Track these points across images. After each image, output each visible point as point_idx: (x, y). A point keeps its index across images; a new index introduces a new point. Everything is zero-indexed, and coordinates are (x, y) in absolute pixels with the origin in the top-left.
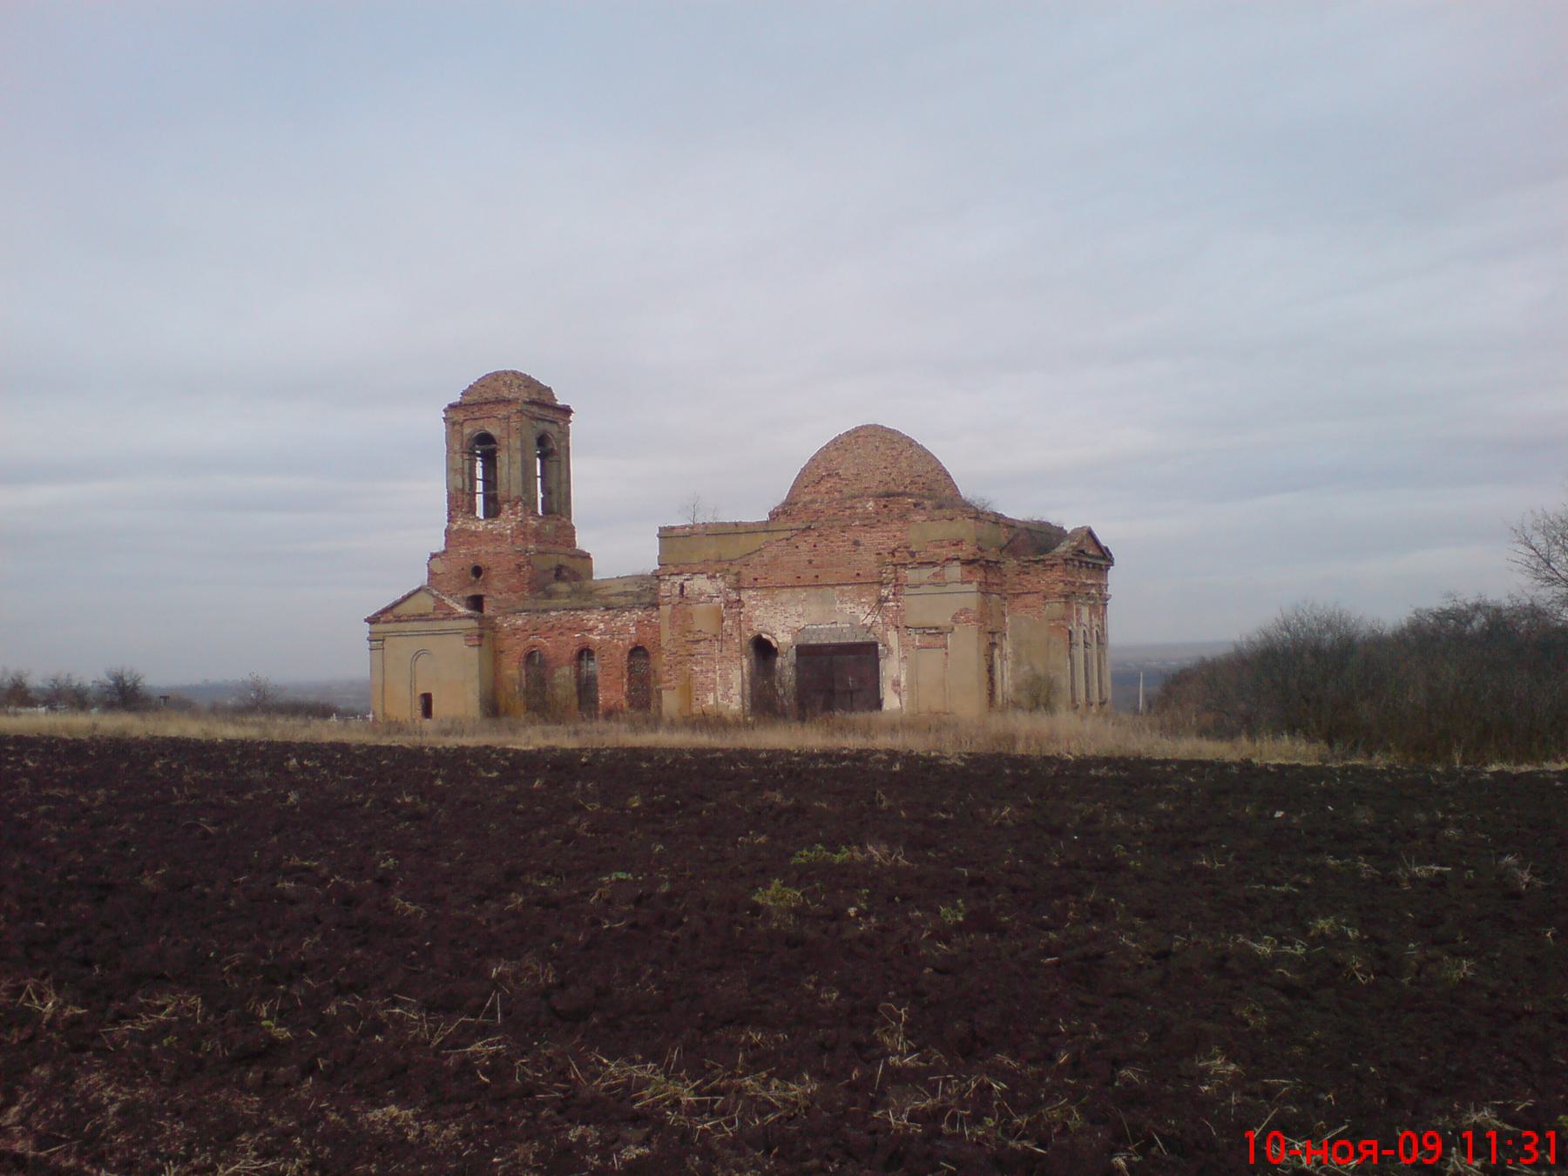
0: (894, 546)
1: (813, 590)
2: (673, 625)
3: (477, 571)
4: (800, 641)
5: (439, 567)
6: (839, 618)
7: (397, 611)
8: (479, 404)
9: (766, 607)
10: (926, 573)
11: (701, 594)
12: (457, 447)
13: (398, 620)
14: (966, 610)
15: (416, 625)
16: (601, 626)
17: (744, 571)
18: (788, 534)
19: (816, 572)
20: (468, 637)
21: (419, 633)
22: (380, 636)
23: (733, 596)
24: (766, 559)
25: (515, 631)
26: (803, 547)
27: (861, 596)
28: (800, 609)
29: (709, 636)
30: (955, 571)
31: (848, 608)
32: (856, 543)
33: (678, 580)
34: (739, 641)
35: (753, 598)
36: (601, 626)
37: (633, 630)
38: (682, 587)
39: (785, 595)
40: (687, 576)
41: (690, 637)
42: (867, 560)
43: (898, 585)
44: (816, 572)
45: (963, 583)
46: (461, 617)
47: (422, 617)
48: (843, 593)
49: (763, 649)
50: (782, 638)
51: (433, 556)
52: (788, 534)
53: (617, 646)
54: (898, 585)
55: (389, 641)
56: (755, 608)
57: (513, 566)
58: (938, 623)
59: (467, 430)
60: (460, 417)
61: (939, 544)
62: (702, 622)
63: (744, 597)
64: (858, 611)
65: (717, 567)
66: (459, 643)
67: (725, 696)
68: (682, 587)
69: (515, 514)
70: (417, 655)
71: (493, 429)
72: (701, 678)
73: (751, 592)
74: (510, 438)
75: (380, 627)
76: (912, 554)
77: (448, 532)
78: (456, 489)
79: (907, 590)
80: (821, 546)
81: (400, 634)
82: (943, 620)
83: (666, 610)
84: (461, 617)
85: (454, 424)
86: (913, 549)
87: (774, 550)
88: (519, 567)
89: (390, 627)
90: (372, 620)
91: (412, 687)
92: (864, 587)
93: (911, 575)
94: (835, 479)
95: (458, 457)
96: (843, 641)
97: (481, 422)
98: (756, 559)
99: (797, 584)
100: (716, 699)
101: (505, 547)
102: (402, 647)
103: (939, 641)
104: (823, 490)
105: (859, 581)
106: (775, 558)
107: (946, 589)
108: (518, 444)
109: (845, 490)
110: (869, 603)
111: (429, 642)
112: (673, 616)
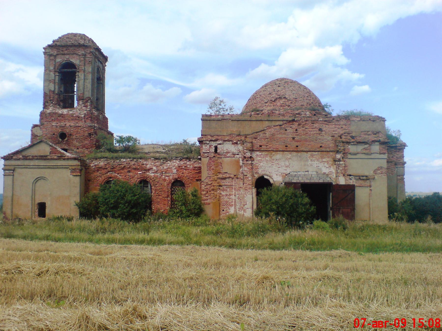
0: (341, 132)
1: (294, 154)
2: (209, 168)
3: (63, 136)
4: (287, 180)
5: (39, 132)
6: (310, 169)
7: (24, 153)
8: (66, 46)
9: (267, 161)
10: (360, 148)
11: (228, 153)
12: (52, 68)
13: (26, 158)
14: (381, 168)
15: (37, 162)
16: (154, 168)
17: (254, 141)
18: (281, 123)
19: (297, 144)
20: (73, 171)
21: (39, 167)
22: (12, 168)
23: (248, 154)
24: (267, 135)
25: (99, 169)
26: (290, 130)
27: (322, 158)
28: (287, 164)
29: (232, 176)
30: (376, 148)
31: (316, 163)
32: (320, 130)
33: (214, 144)
34: (250, 180)
35: (260, 156)
36: (154, 168)
37: (175, 171)
38: (216, 148)
39: (278, 156)
40: (220, 142)
41: (220, 176)
42: (327, 140)
43: (345, 154)
44: (297, 144)
45: (380, 154)
46: (68, 159)
47: (43, 158)
48: (312, 156)
49: (262, 183)
50: (276, 178)
51: (35, 126)
52: (281, 123)
53: (165, 180)
54: (345, 154)
55: (18, 170)
56: (260, 161)
57: (86, 134)
58: (367, 174)
59: (58, 60)
60: (55, 52)
61: (366, 133)
62: (227, 167)
63: (254, 155)
64: (321, 165)
65: (238, 138)
66: (67, 173)
67: (241, 208)
68: (216, 148)
69: (86, 106)
70: (37, 180)
71: (75, 61)
72: (226, 199)
73: (258, 153)
74: (74, 68)
75: (13, 162)
76: (353, 137)
77: (42, 114)
78: (50, 91)
79: (349, 156)
80: (300, 130)
81: (26, 167)
82: (368, 172)
83: (205, 160)
84: (68, 159)
85: (51, 55)
86: (353, 134)
87: (272, 130)
88: (90, 134)
89: (19, 163)
90: (6, 158)
91: (33, 199)
92: (325, 153)
93: (352, 148)
94: (284, 100)
95: (52, 74)
96: (312, 181)
97: (67, 57)
98: (261, 134)
99: (286, 149)
100: (235, 210)
101: (81, 124)
102: (26, 176)
103: (367, 183)
104: (279, 104)
105: (322, 150)
106: (273, 135)
107: (372, 156)
108: (90, 70)
109: (292, 105)
110: (328, 162)
111: (46, 173)
112: (209, 164)
